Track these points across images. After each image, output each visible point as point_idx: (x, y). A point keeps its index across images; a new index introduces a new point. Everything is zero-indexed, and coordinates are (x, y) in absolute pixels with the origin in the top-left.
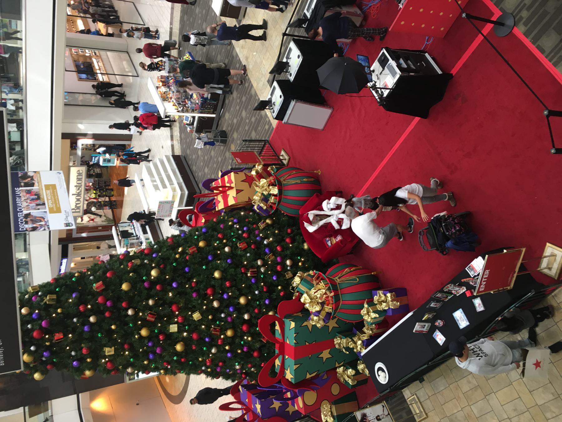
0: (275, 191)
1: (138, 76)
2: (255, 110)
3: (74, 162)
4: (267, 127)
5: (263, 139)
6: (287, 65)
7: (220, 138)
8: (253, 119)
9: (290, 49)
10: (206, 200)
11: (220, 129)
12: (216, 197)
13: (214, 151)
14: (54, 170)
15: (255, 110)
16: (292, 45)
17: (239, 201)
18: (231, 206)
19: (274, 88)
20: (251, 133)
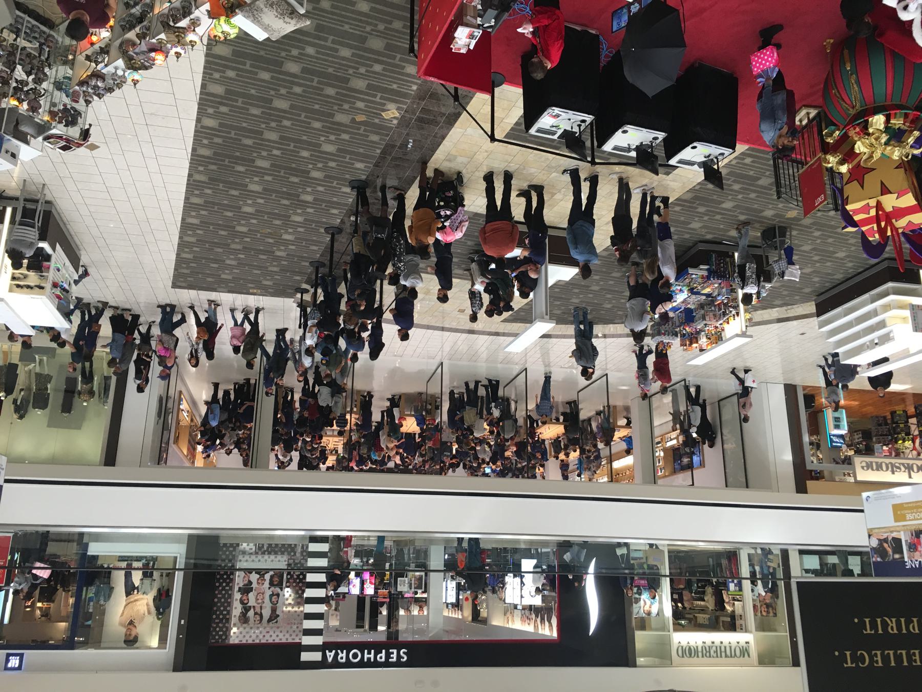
0: (878, 121)
1: (526, 369)
2: (722, 188)
3: (845, 475)
4: (748, 160)
5: (771, 162)
6: (640, 149)
7: (778, 239)
8: (736, 187)
9: (615, 148)
10: (906, 246)
11: (759, 242)
12: (900, 231)
13: (803, 244)
15: (722, 188)
16: (608, 147)
17: (906, 185)
18: (916, 199)
19: (680, 162)
20: (762, 187)
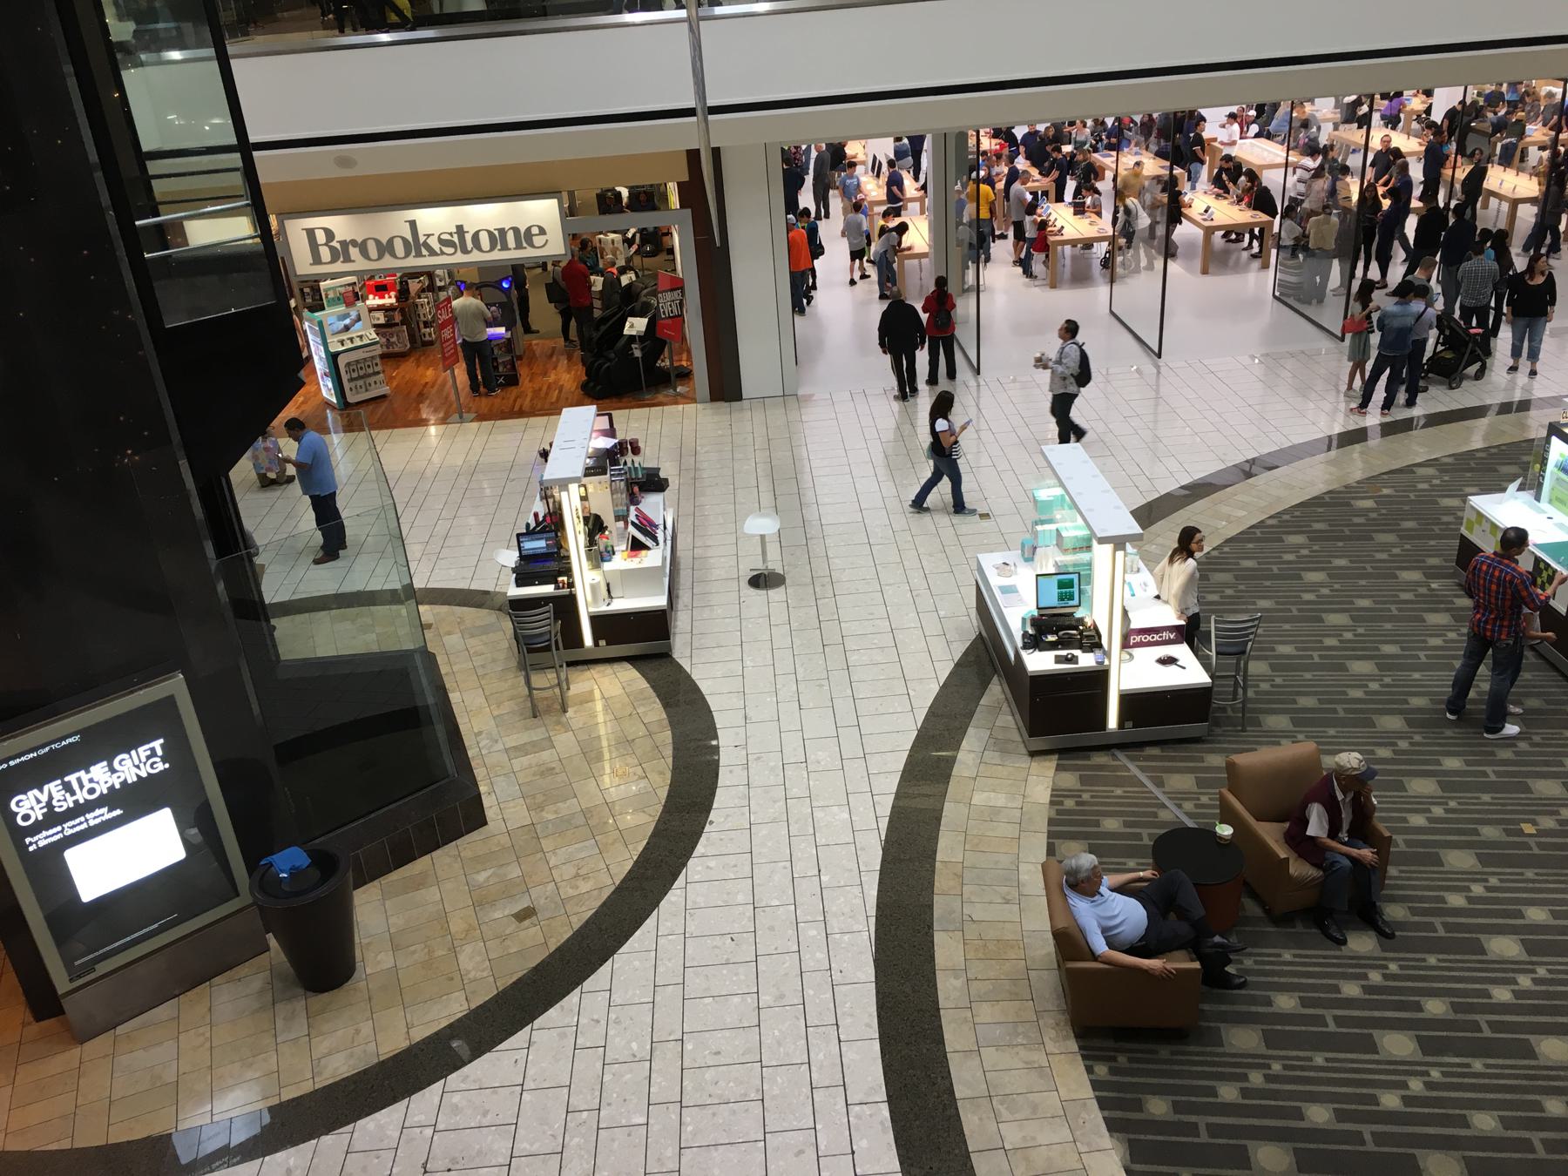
14: (1556, 501)
